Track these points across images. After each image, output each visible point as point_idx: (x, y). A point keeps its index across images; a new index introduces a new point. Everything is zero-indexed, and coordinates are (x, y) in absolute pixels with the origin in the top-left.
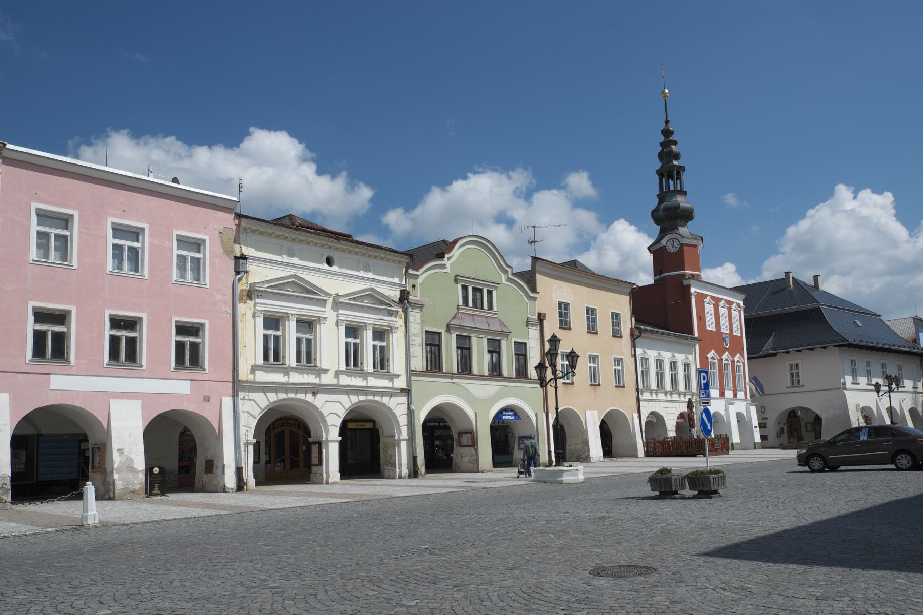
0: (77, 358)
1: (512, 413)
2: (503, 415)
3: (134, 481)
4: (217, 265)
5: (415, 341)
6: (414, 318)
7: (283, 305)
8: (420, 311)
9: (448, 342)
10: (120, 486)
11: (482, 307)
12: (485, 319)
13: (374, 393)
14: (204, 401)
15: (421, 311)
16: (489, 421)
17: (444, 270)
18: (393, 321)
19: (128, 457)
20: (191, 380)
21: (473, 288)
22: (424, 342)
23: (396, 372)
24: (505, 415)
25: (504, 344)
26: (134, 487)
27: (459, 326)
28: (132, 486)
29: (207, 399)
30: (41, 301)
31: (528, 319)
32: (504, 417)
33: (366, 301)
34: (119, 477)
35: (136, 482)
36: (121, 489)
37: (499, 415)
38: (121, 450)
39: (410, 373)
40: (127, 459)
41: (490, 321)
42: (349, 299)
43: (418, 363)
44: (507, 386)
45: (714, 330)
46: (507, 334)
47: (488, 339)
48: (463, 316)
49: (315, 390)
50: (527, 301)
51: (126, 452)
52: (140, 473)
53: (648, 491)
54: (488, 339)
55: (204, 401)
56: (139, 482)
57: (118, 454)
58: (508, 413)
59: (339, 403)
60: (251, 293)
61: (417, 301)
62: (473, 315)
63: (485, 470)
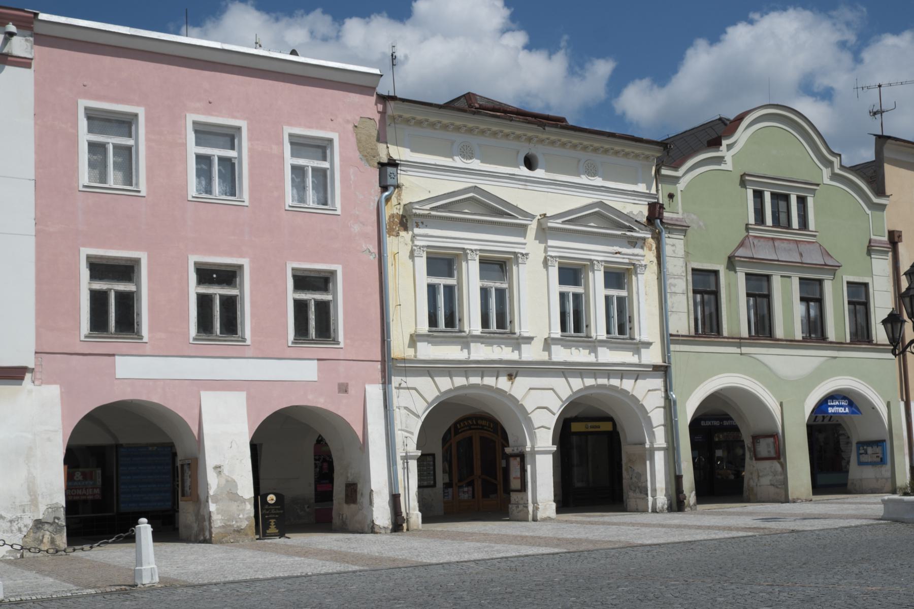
0: (151, 330)
3: (239, 515)
4: (352, 177)
6: (673, 248)
8: (682, 237)
9: (730, 286)
10: (219, 522)
11: (789, 225)
13: (609, 374)
14: (340, 391)
15: (685, 236)
17: (723, 167)
18: (637, 255)
19: (229, 479)
20: (318, 360)
23: (645, 338)
24: (833, 406)
26: (238, 524)
28: (236, 522)
29: (343, 389)
30: (98, 246)
32: (830, 410)
33: (592, 224)
34: (217, 509)
35: (241, 516)
36: (220, 527)
37: (823, 406)
38: (218, 468)
39: (669, 339)
40: (227, 481)
41: (802, 247)
42: (564, 222)
43: (681, 323)
44: (835, 358)
46: (833, 269)
48: (756, 241)
49: (513, 371)
50: (869, 212)
51: (226, 471)
52: (247, 503)
55: (340, 391)
56: (246, 516)
57: (215, 475)
58: (837, 403)
59: (552, 391)
60: (407, 220)
62: (773, 239)
63: (798, 499)
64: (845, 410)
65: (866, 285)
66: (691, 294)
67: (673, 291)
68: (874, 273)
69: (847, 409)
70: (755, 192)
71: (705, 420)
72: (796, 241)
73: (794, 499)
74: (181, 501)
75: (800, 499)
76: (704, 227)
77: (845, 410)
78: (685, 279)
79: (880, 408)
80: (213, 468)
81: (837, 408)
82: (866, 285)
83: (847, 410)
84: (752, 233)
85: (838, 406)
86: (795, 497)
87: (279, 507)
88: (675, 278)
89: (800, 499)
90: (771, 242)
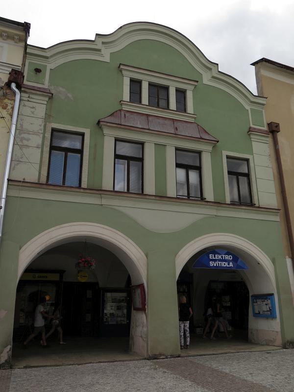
1: (227, 257)
2: (212, 260)
5: (28, 140)
7: (83, 169)
11: (168, 108)
12: (171, 122)
16: (175, 273)
21: (151, 85)
22: (47, 143)
24: (215, 260)
25: (207, 162)
27: (118, 124)
31: (249, 129)
41: (178, 124)
45: (189, 322)
47: (177, 149)
48: (127, 115)
53: (266, 128)
54: (177, 149)
58: (220, 257)
61: (44, 88)
62: (148, 115)
63: (161, 355)
64: (229, 264)
65: (247, 160)
66: (47, 149)
67: (25, 144)
68: (254, 152)
69: (231, 263)
70: (132, 81)
71: (215, 253)
72: (173, 119)
73: (155, 355)
74: (118, 164)
75: (163, 355)
76: (72, 98)
77: (229, 264)
78: (41, 136)
79: (266, 265)
80: (41, 71)
81: (220, 263)
82: (247, 160)
83: (231, 265)
84: (125, 108)
85: (220, 260)
86: (157, 353)
87: (190, 309)
88: (29, 134)
89: (163, 355)
90: (144, 117)
